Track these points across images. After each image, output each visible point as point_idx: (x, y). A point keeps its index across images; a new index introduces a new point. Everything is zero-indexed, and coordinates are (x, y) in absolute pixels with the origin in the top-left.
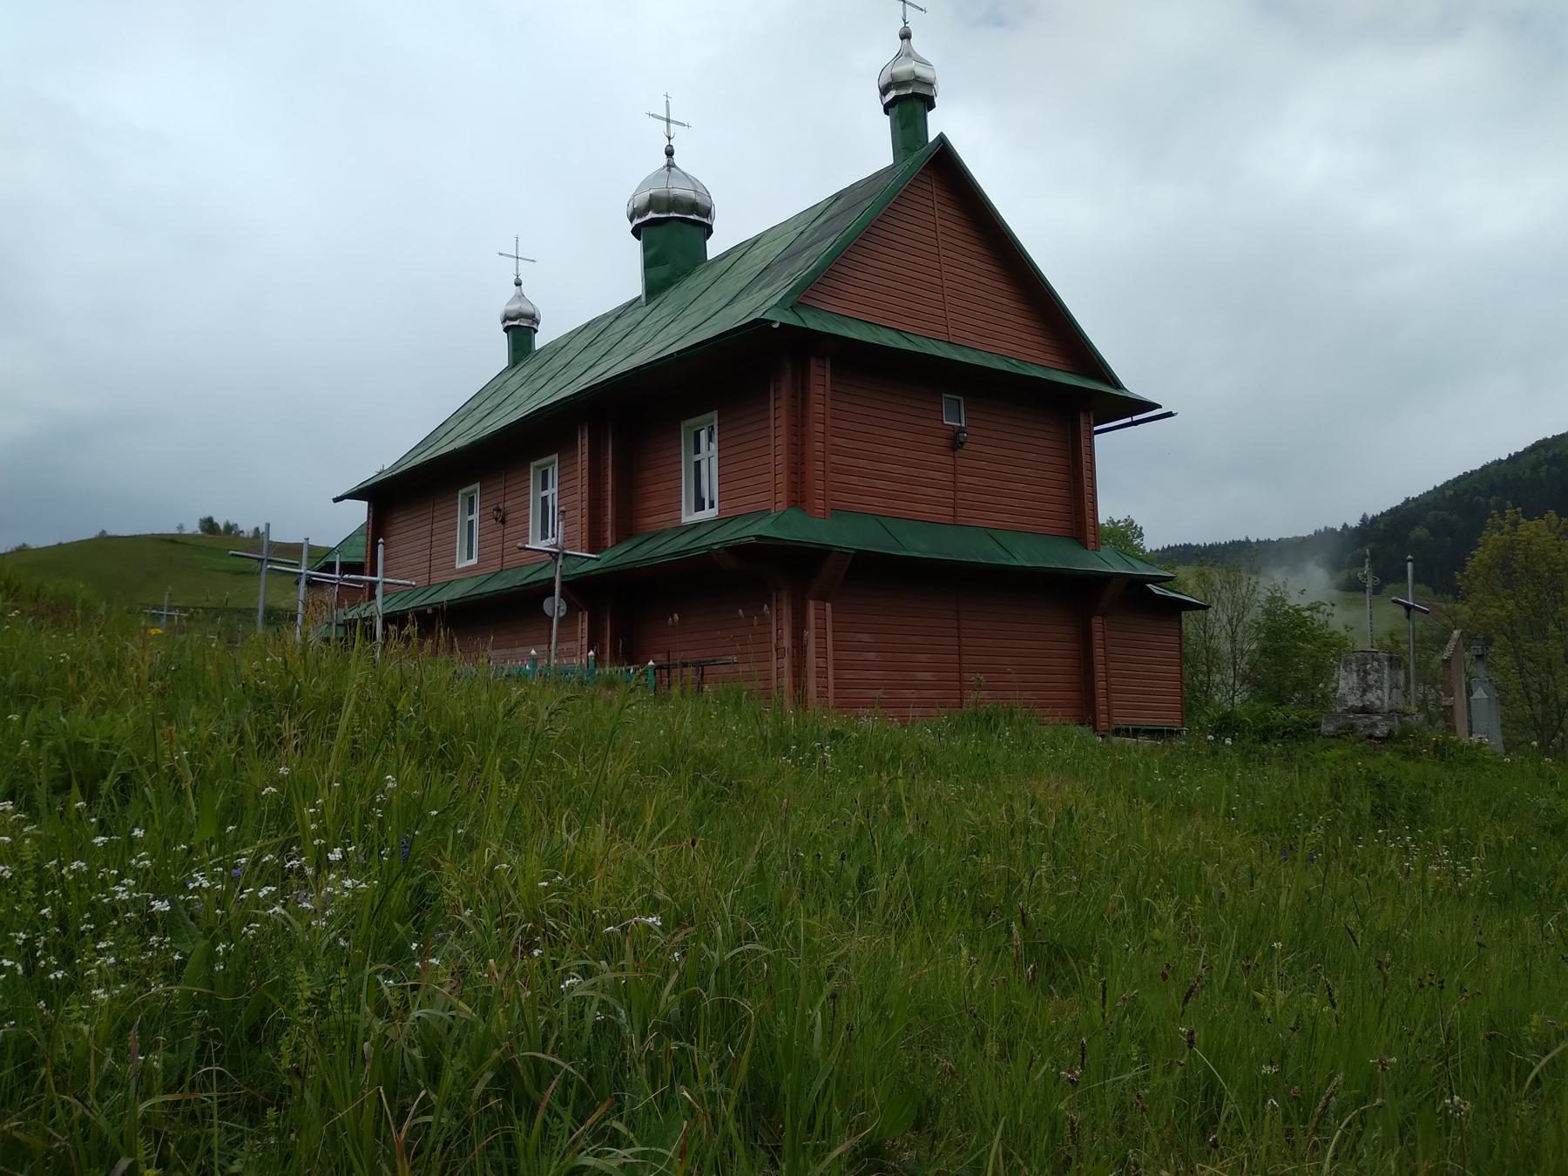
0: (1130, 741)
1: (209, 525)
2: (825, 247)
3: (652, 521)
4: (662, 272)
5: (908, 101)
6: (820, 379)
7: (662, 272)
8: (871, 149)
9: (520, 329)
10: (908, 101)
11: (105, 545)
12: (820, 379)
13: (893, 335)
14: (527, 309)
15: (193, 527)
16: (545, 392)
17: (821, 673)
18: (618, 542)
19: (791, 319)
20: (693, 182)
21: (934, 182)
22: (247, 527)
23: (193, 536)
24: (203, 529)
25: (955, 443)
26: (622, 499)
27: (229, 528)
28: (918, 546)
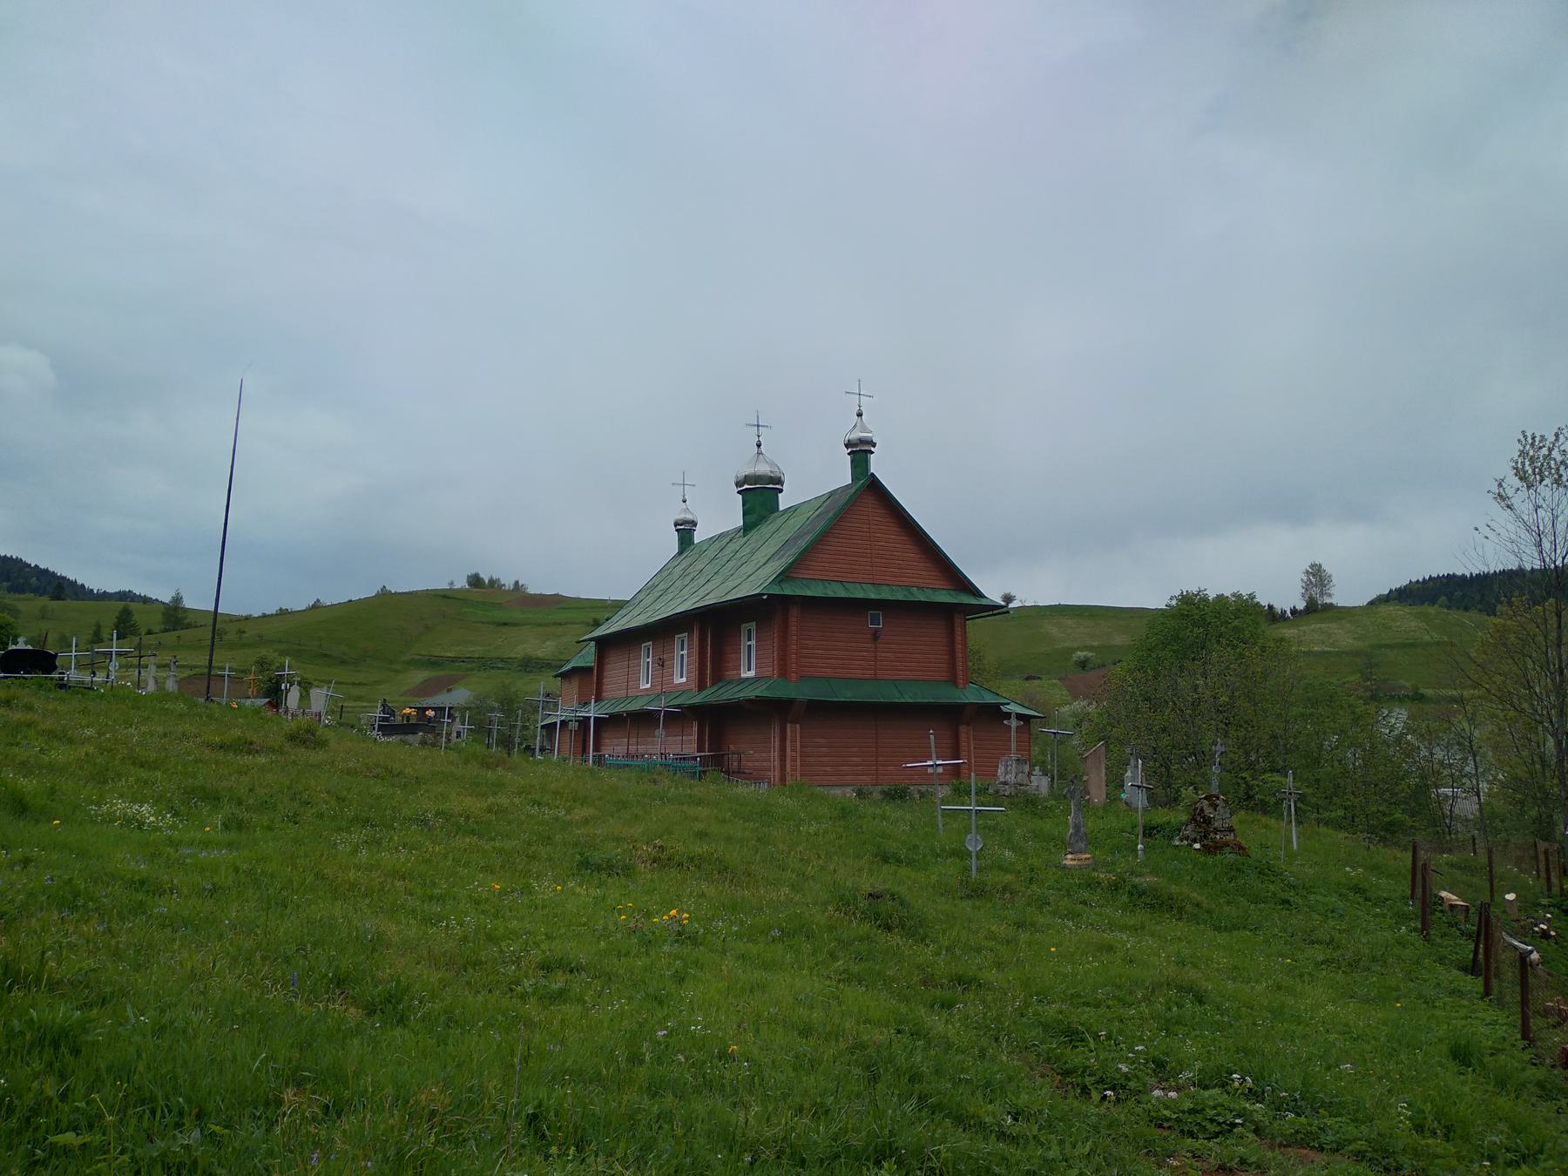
0: (221, 756)
1: (475, 581)
2: (808, 538)
3: (730, 674)
4: (753, 518)
5: (860, 451)
6: (794, 613)
7: (753, 518)
8: (841, 475)
9: (685, 531)
10: (860, 451)
11: (385, 600)
12: (794, 613)
13: (837, 586)
14: (689, 517)
15: (461, 583)
16: (673, 604)
17: (794, 760)
18: (713, 684)
19: (776, 591)
20: (772, 464)
21: (869, 494)
22: (508, 582)
23: (461, 590)
24: (470, 584)
25: (875, 636)
26: (714, 666)
27: (492, 582)
28: (846, 695)
